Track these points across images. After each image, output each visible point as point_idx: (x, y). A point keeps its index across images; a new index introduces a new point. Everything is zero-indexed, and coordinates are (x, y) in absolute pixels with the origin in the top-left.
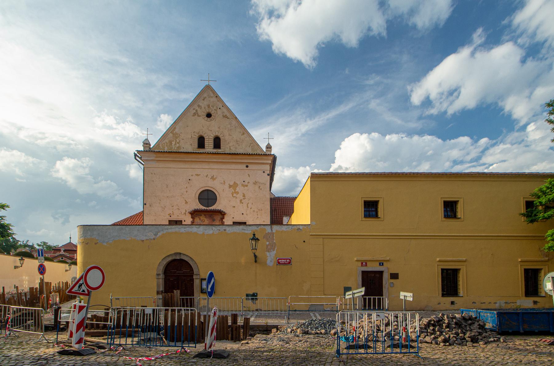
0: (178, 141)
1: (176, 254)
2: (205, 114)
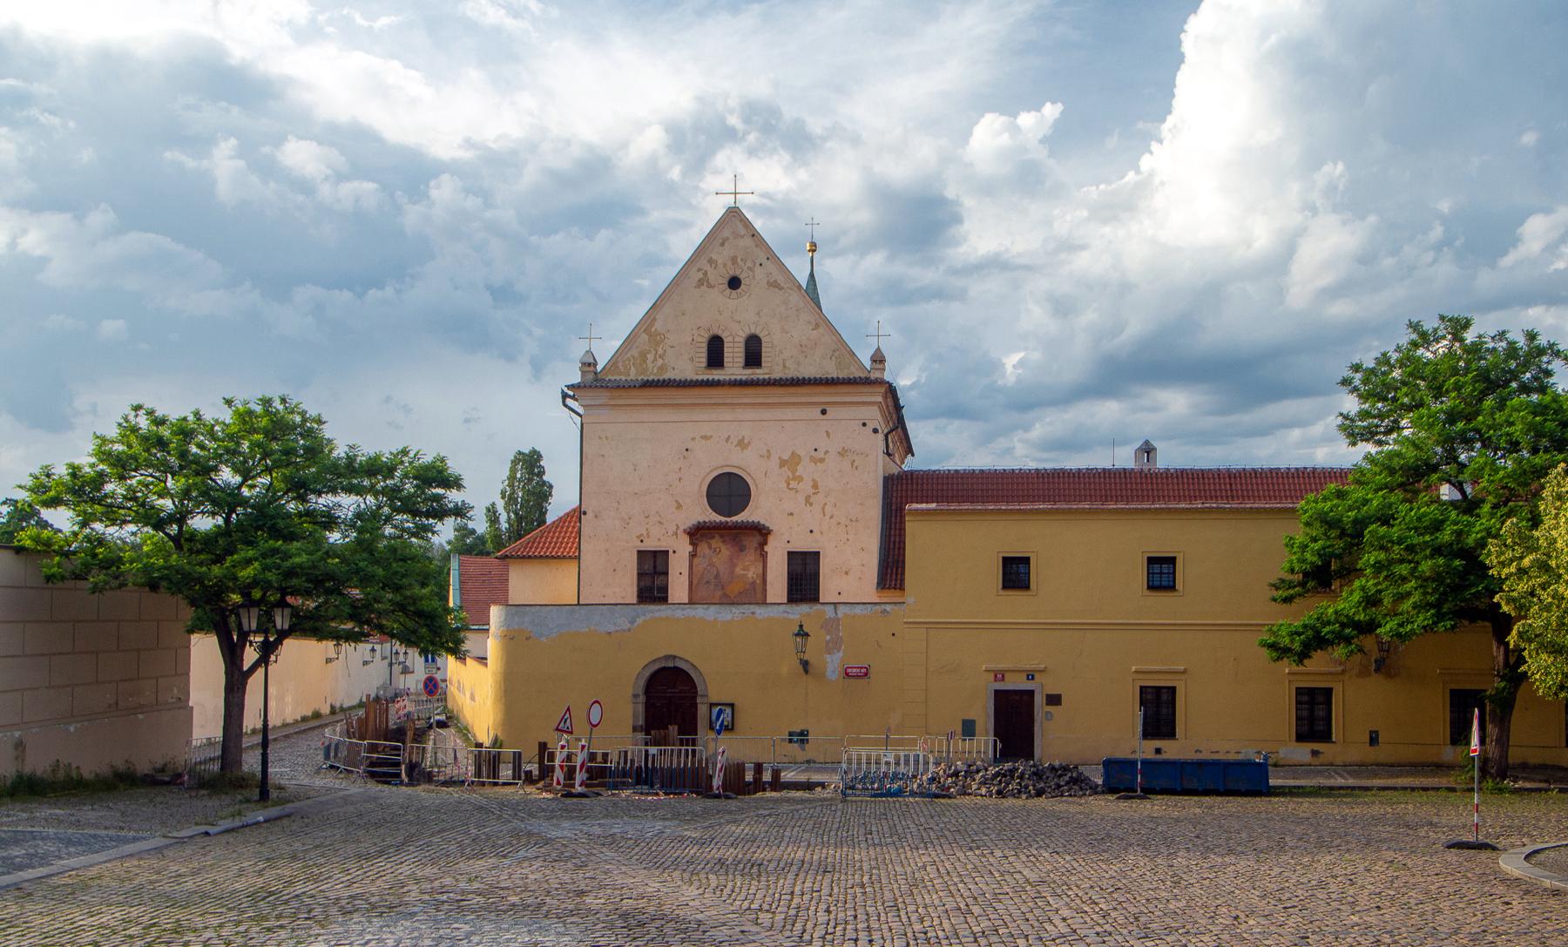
0: (660, 351)
1: (667, 657)
2: (726, 281)
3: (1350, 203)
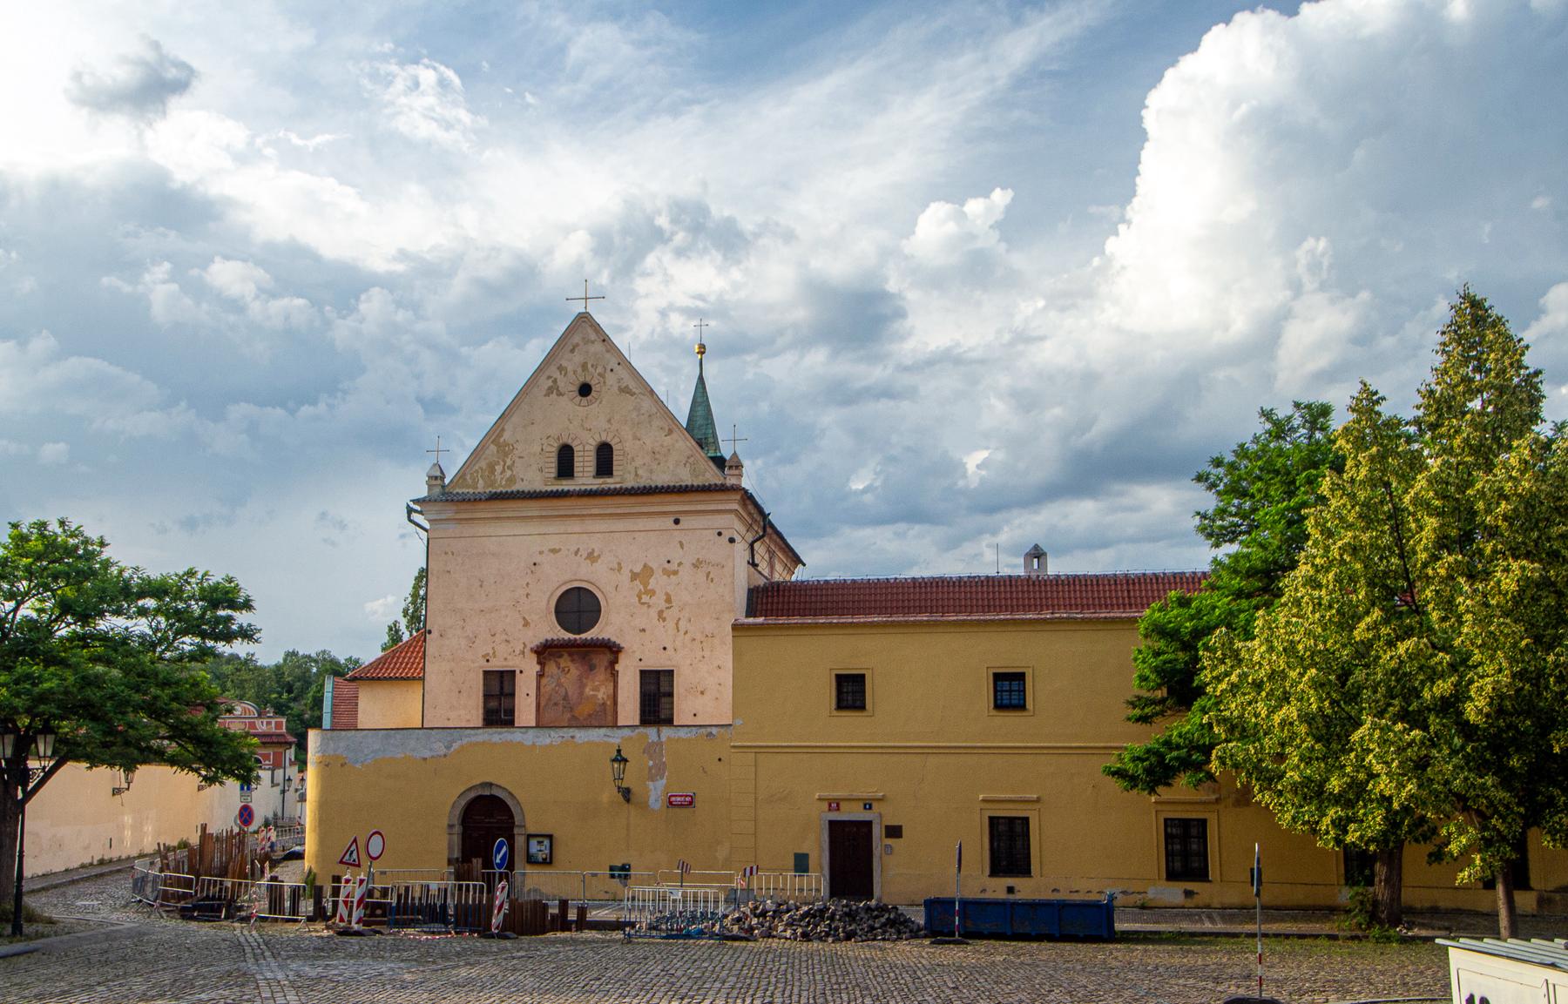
0: (509, 462)
2: (576, 388)
3: (1342, 278)
